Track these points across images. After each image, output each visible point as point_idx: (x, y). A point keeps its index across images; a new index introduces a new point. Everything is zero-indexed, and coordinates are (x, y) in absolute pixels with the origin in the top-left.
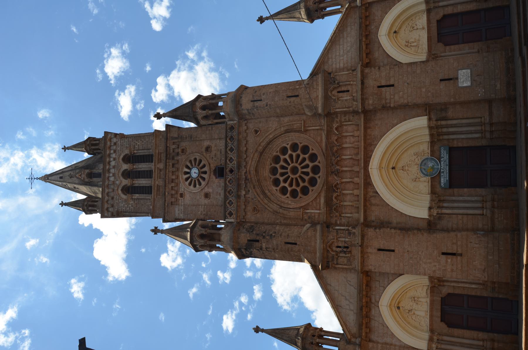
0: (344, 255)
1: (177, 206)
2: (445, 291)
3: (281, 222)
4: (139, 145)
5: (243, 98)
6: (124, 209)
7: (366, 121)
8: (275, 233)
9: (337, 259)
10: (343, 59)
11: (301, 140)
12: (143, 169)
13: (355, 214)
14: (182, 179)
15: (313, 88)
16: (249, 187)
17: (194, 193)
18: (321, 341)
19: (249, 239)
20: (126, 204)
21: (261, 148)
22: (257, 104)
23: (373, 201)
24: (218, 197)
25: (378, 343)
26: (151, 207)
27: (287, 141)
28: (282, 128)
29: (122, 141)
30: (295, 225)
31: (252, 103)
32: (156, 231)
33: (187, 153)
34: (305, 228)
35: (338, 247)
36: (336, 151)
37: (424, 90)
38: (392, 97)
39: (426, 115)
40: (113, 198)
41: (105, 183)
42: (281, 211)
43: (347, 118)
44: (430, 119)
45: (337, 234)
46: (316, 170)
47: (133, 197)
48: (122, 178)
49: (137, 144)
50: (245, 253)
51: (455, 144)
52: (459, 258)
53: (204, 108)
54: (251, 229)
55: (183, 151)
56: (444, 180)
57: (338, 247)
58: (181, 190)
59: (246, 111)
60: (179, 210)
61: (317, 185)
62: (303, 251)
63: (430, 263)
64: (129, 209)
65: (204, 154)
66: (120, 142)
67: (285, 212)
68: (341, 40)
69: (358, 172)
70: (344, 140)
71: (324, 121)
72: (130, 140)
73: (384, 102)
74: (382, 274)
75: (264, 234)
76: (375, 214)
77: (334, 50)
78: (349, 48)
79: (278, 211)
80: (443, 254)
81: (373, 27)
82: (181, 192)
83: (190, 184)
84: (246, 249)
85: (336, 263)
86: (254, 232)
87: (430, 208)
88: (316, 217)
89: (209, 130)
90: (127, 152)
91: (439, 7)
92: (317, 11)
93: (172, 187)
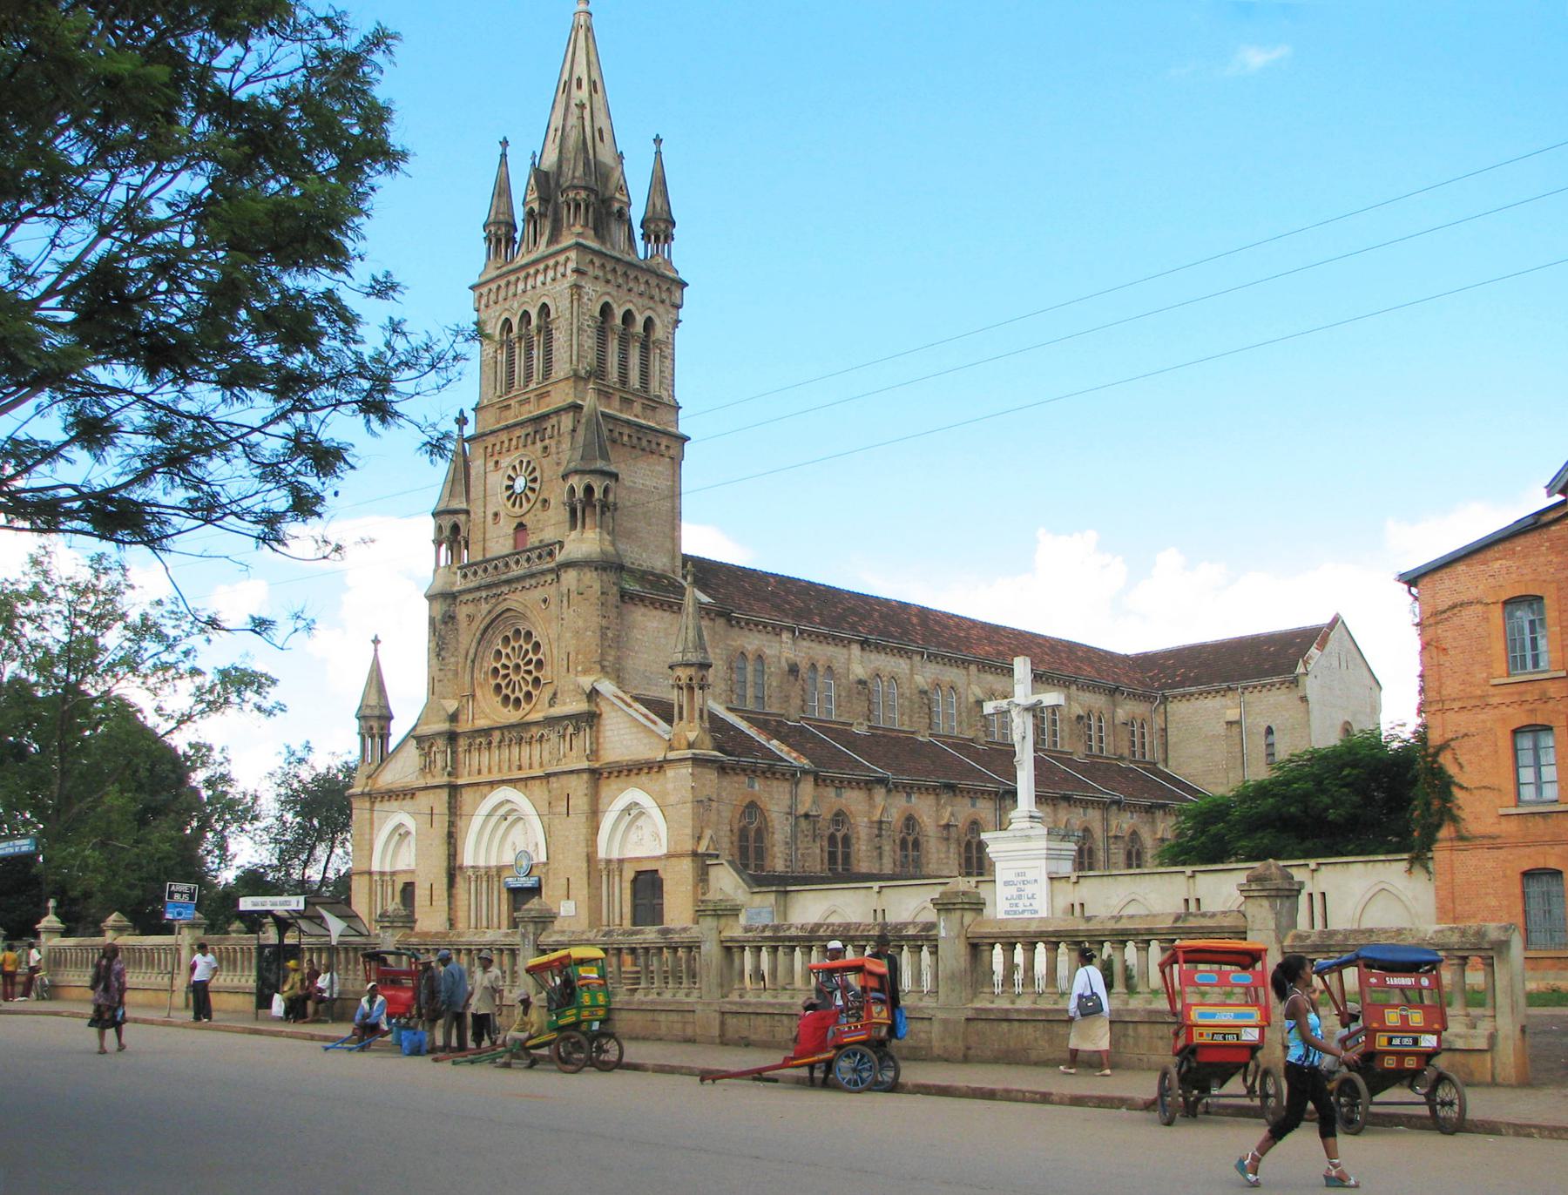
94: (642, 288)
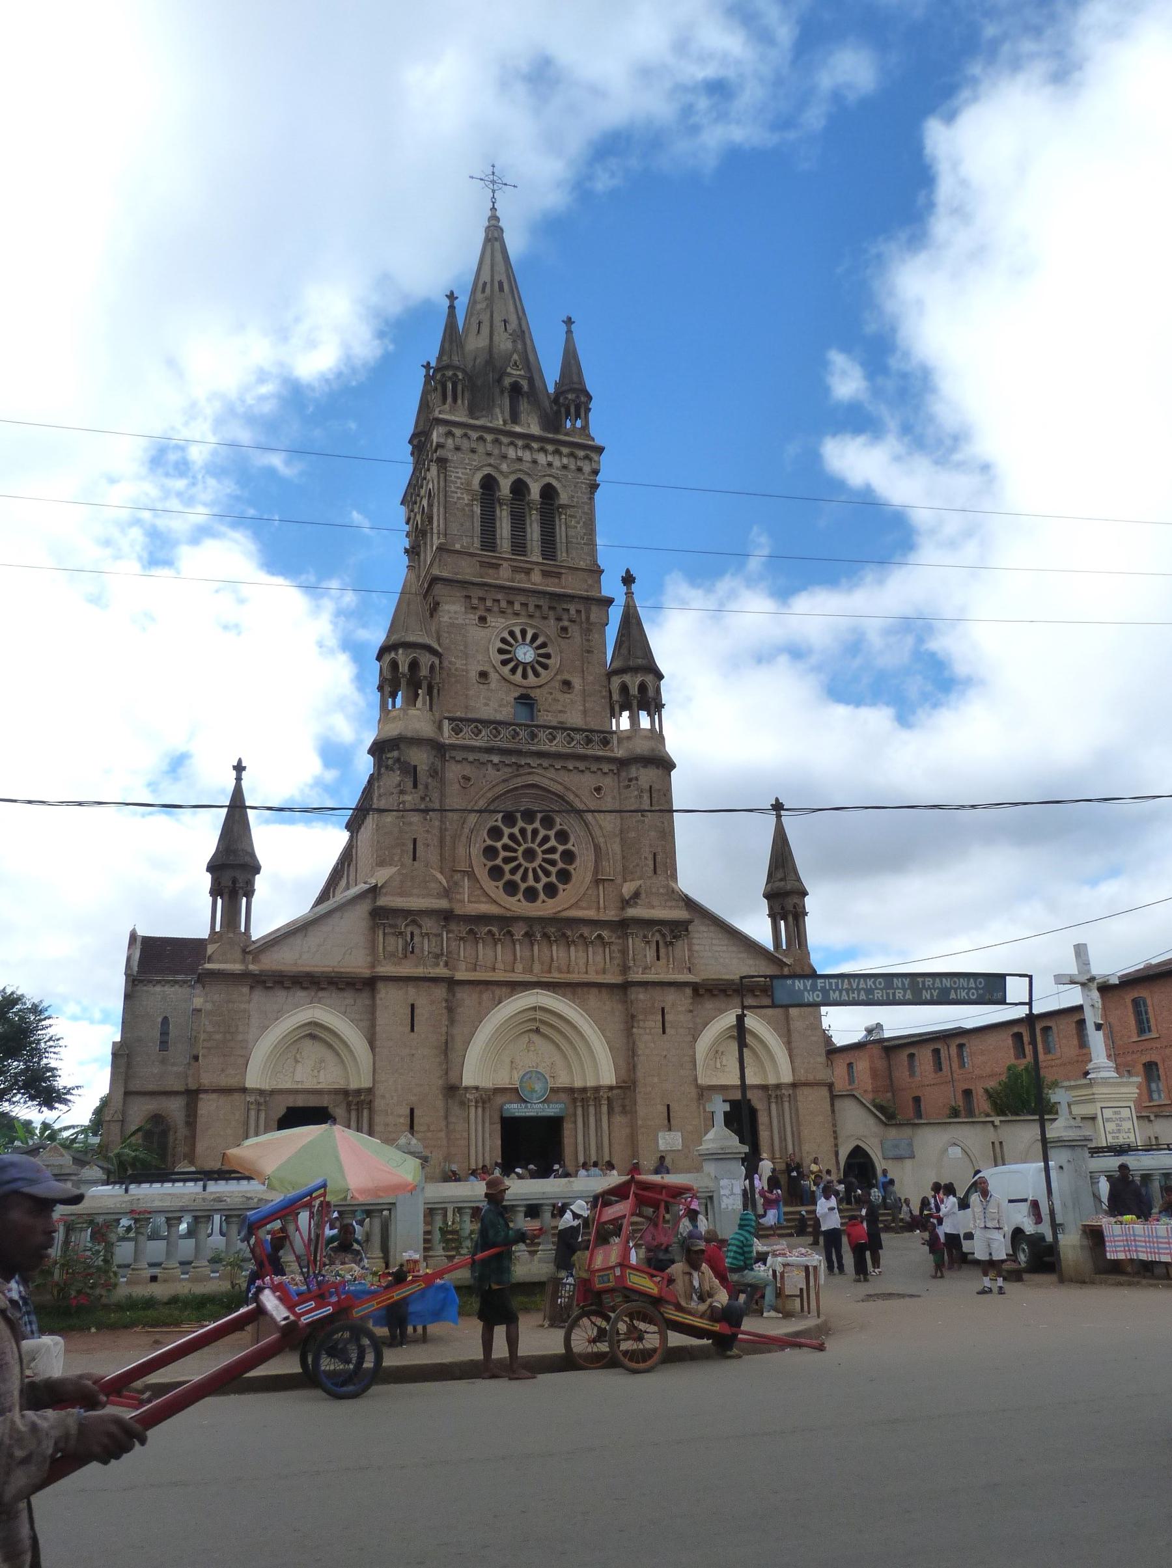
1: (463, 609)
3: (446, 830)
4: (576, 527)
7: (610, 987)
8: (431, 820)
9: (393, 934)
10: (706, 951)
11: (582, 871)
12: (529, 530)
14: (515, 625)
15: (666, 901)
16: (506, 770)
17: (488, 650)
22: (645, 798)
23: (486, 996)
28: (603, 840)
29: (583, 486)
30: (441, 855)
33: (560, 639)
34: (439, 876)
35: (412, 934)
36: (564, 935)
38: (648, 1031)
40: (473, 451)
41: (503, 435)
42: (466, 831)
43: (617, 955)
44: (611, 1088)
45: (436, 935)
46: (531, 894)
49: (579, 523)
50: (388, 756)
51: (567, 1127)
53: (643, 687)
54: (434, 773)
55: (564, 629)
56: (516, 1109)
57: (412, 934)
58: (492, 620)
59: (634, 775)
62: (404, 872)
64: (453, 489)
65: (559, 677)
67: (464, 839)
69: (531, 971)
71: (613, 916)
73: (641, 1017)
74: (372, 1011)
75: (428, 799)
77: (720, 935)
78: (722, 960)
79: (465, 826)
80: (412, 1110)
82: (488, 619)
84: (398, 760)
85: (386, 931)
86: (430, 780)
87: (477, 1088)
88: (458, 897)
90: (564, 498)
91: (769, 1103)
92: (783, 908)
93: (498, 601)
94: (489, 447)
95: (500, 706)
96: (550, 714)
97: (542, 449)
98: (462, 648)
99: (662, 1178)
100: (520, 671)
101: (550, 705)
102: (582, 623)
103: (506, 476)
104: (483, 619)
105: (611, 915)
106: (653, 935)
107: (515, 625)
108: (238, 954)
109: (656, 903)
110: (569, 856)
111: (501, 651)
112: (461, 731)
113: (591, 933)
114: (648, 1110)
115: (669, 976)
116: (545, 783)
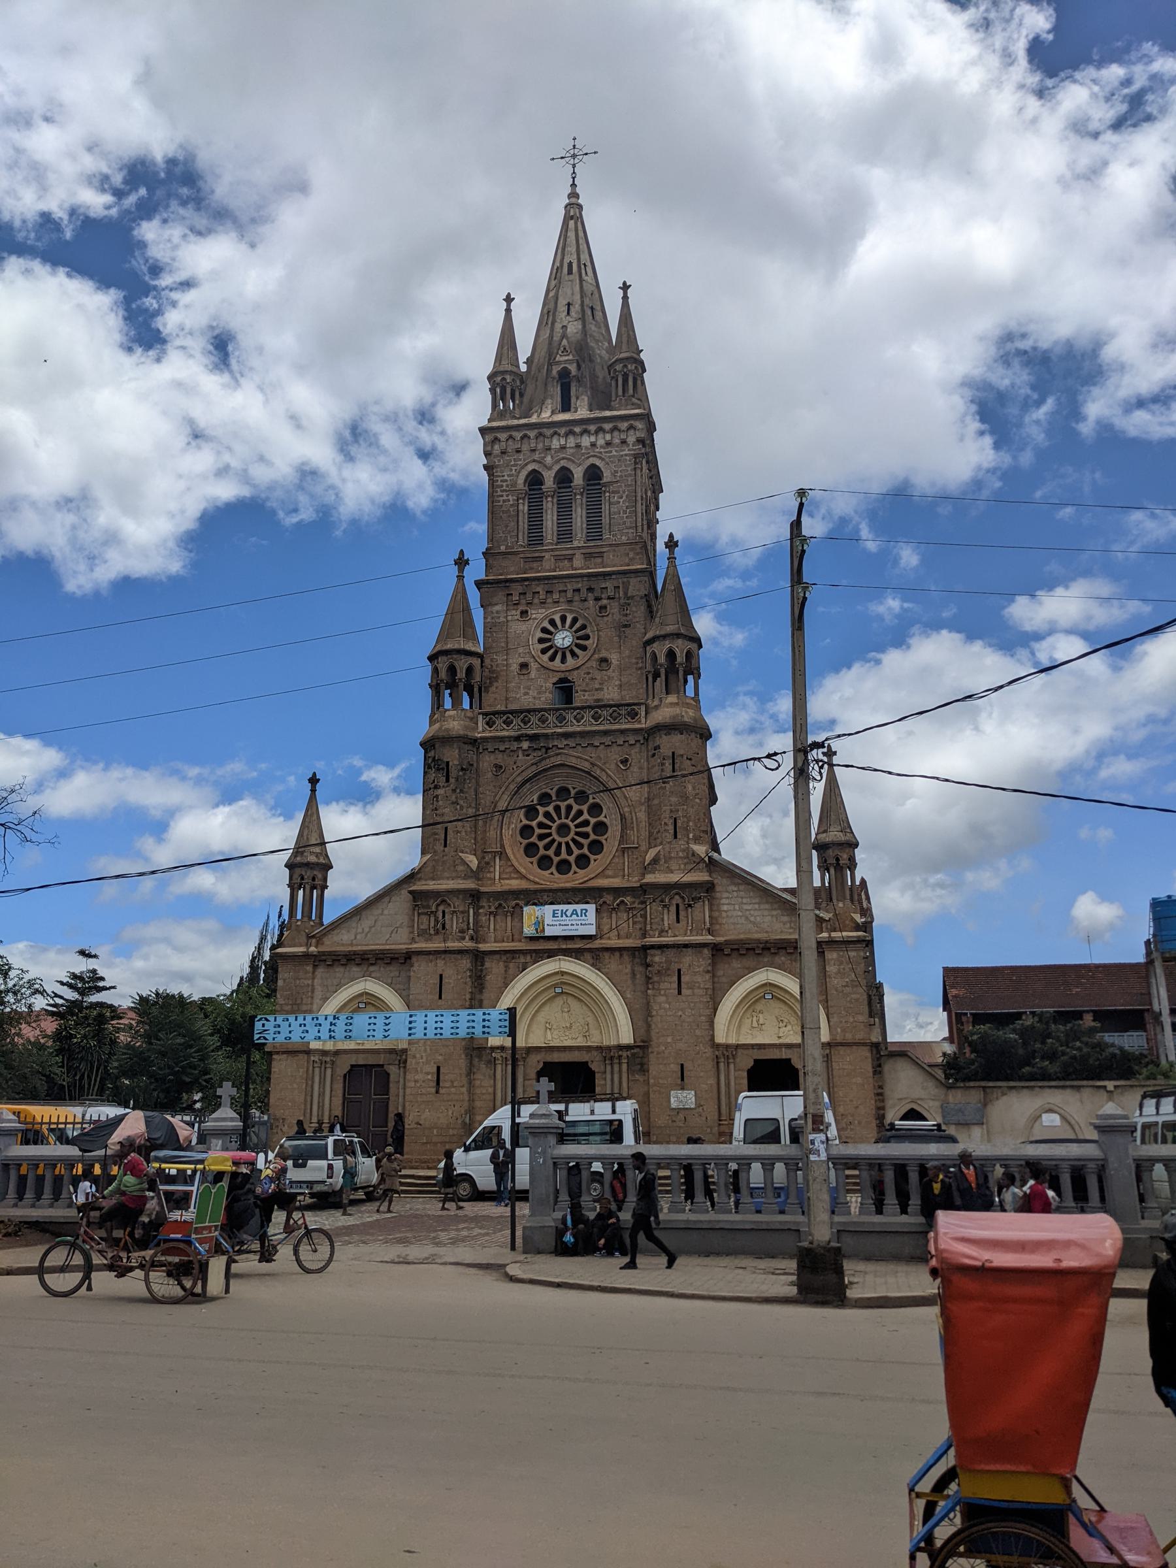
0: (432, 925)
2: (393, 1070)
5: (679, 736)
6: (499, 483)
7: (632, 951)
9: (426, 914)
10: (735, 910)
11: (611, 841)
13: (493, 935)
18: (308, 887)
19: (451, 764)
20: (507, 486)
21: (598, 772)
24: (522, 691)
25: (313, 979)
26: (503, 548)
27: (609, 816)
31: (671, 754)
32: (462, 562)
33: (598, 618)
35: (444, 912)
37: (669, 1040)
39: (635, 1042)
40: (518, 451)
45: (462, 912)
47: (521, 501)
48: (556, 468)
52: (434, 1090)
60: (497, 612)
61: (540, 871)
63: (425, 1051)
66: (626, 455)
68: (767, 906)
70: (605, 915)
72: (630, 479)
73: (656, 979)
75: (458, 791)
76: (494, 968)
78: (752, 919)
80: (438, 1068)
81: (783, 958)
83: (541, 641)
89: (637, 663)
90: (607, 476)
95: (539, 693)
96: (587, 694)
97: (585, 431)
98: (503, 644)
99: (592, 1112)
100: (568, 655)
101: (587, 684)
102: (620, 598)
103: (550, 469)
104: (524, 613)
105: (634, 882)
106: (671, 898)
107: (554, 613)
108: (304, 939)
109: (674, 866)
110: (601, 828)
111: (541, 641)
112: (494, 723)
113: (615, 899)
114: (661, 1068)
115: (686, 938)
116: (573, 761)
